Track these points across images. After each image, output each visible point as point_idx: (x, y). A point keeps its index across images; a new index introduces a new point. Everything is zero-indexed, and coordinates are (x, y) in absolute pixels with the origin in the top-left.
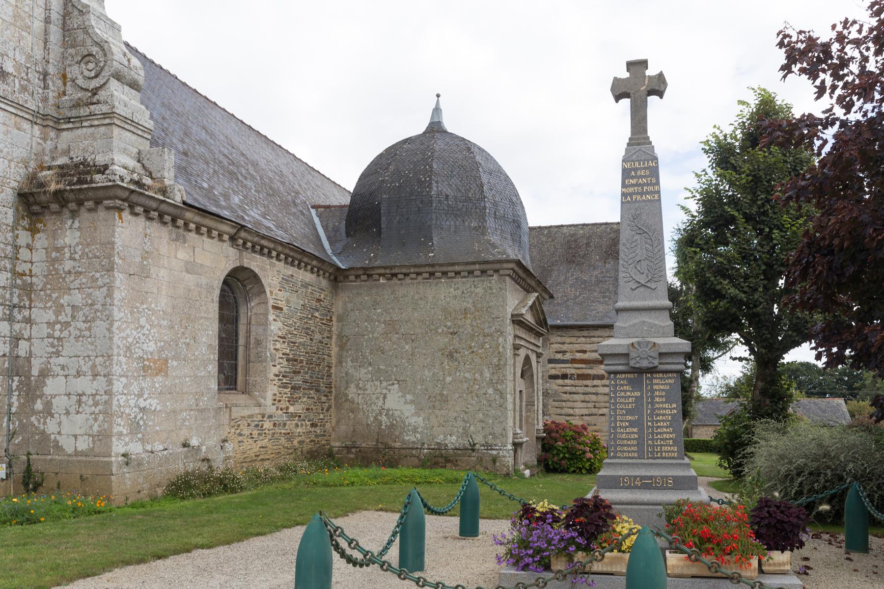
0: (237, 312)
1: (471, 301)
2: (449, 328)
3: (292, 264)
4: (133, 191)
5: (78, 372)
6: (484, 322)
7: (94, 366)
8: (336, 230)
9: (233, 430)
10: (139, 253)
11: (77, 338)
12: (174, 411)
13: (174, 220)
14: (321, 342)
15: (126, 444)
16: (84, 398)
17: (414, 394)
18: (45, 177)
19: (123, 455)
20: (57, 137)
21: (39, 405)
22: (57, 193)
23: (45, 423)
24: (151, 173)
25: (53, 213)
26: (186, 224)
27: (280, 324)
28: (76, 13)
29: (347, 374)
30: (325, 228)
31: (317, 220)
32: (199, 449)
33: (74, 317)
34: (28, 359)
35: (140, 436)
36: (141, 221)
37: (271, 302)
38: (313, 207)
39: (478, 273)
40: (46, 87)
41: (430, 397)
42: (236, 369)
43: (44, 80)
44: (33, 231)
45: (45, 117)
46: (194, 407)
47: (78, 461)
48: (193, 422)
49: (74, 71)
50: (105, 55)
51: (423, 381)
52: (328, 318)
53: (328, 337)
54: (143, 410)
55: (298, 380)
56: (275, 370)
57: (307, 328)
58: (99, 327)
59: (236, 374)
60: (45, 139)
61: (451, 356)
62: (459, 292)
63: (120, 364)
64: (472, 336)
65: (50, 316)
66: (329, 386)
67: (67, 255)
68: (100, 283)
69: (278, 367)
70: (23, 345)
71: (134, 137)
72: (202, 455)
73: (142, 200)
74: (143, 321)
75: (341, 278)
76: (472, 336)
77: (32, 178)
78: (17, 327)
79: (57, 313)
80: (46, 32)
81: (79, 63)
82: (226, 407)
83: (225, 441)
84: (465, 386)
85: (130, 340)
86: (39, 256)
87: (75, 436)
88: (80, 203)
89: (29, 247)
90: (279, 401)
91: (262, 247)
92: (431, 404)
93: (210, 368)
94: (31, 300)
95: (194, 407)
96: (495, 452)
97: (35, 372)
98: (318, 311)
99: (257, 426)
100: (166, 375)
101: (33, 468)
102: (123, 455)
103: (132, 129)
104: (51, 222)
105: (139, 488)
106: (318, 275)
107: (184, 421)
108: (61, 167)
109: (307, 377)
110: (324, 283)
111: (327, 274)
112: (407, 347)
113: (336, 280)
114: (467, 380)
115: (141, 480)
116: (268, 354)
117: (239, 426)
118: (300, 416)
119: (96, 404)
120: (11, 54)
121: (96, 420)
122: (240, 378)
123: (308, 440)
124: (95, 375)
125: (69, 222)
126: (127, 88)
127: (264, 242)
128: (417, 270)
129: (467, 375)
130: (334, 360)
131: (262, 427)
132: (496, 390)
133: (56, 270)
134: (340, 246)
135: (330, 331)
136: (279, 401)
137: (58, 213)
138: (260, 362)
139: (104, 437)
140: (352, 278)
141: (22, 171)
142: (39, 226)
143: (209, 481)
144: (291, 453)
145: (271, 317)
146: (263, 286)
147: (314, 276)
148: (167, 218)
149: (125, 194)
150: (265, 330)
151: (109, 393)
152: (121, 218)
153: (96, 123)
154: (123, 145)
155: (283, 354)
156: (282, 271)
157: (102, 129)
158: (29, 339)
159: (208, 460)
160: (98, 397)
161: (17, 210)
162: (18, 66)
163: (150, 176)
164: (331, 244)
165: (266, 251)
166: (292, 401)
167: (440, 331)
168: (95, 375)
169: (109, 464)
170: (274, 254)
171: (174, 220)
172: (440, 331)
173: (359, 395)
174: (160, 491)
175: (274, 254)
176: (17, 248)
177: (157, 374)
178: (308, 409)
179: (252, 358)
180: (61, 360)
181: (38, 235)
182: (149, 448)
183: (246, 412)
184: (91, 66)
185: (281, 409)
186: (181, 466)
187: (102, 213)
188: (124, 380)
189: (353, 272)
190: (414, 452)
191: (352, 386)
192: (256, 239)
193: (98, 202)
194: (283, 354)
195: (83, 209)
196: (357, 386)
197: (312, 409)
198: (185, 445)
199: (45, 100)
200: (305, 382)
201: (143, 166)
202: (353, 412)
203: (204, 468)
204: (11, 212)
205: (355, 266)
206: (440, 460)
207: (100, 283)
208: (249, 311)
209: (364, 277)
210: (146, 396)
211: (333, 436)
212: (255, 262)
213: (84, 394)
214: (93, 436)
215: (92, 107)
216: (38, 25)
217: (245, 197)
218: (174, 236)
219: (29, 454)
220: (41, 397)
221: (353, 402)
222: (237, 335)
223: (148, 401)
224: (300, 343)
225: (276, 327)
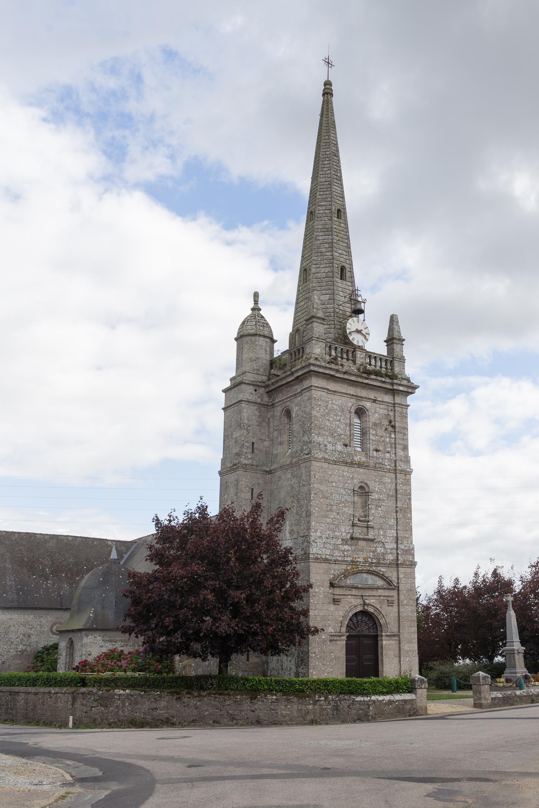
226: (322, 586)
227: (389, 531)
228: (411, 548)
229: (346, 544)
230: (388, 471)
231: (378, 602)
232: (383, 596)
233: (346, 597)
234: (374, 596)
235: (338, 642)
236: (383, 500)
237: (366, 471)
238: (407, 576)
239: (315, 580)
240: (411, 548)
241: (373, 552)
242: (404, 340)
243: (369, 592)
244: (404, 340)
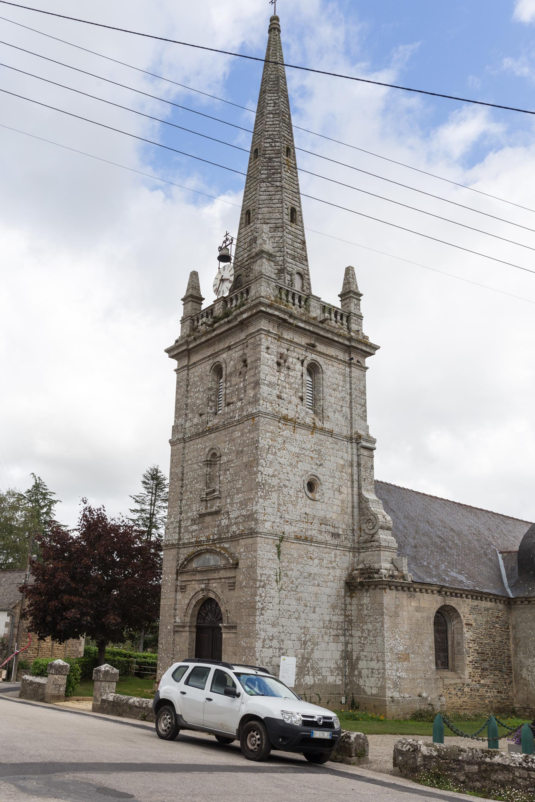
0: (446, 627)
3: (477, 599)
4: (389, 581)
5: (371, 659)
7: (377, 657)
8: (513, 569)
9: (445, 691)
10: (394, 606)
11: (370, 644)
12: (413, 679)
13: (409, 589)
14: (501, 642)
15: (392, 693)
16: (374, 671)
18: (355, 574)
19: (391, 697)
20: (359, 555)
21: (356, 673)
22: (360, 582)
23: (359, 681)
24: (397, 569)
25: (359, 590)
26: (415, 590)
27: (471, 633)
28: (364, 501)
29: (520, 661)
30: (506, 568)
31: (501, 562)
32: (426, 698)
33: (369, 635)
34: (351, 652)
35: (398, 689)
36: (394, 592)
37: (464, 622)
38: (500, 553)
40: (354, 535)
42: (448, 658)
43: (353, 532)
44: (351, 597)
45: (354, 548)
46: (423, 677)
47: (373, 699)
48: (423, 685)
49: (364, 526)
50: (376, 519)
52: (506, 627)
53: (506, 639)
54: (399, 677)
55: (486, 665)
56: (470, 659)
57: (490, 634)
58: (379, 639)
59: (448, 661)
60: (354, 557)
63: (388, 656)
65: (359, 634)
66: (510, 669)
67: (365, 608)
68: (378, 620)
69: (472, 657)
70: (349, 645)
71: (390, 553)
72: (429, 702)
73: (394, 584)
74: (397, 636)
75: (512, 603)
77: (350, 575)
78: (347, 638)
79: (362, 633)
80: (353, 512)
81: (366, 523)
82: (441, 678)
83: (441, 696)
85: (392, 645)
86: (354, 607)
87: (371, 687)
88: (369, 586)
89: (350, 604)
90: (474, 676)
91: (456, 594)
93: (431, 658)
94: (351, 626)
95: (423, 677)
97: (354, 658)
98: (497, 623)
99: (460, 689)
100: (409, 661)
101: (355, 700)
102: (391, 697)
103: (389, 550)
104: (358, 594)
105: (398, 713)
106: (496, 603)
107: (419, 684)
108: (361, 569)
109: (492, 663)
110: (501, 606)
111: (502, 601)
113: (509, 603)
115: (399, 710)
116: (464, 650)
117: (449, 688)
118: (489, 686)
119: (379, 674)
120: (341, 527)
121: (379, 680)
122: (450, 663)
123: (496, 701)
124: (378, 661)
125: (365, 594)
126: (385, 531)
127: (456, 591)
130: (512, 653)
131: (463, 690)
133: (361, 614)
134: (513, 581)
135: (508, 635)
136: (474, 676)
137: (361, 590)
138: (460, 654)
139: (382, 688)
140: (519, 603)
141: (346, 573)
142: (354, 595)
143: (432, 715)
144: (484, 708)
145: (465, 630)
146: (458, 613)
147: (493, 604)
148: (406, 589)
149: (387, 583)
150: (462, 637)
151: (384, 669)
152: (385, 592)
153: (374, 549)
154: (385, 558)
155: (474, 650)
156: (471, 604)
157: (376, 552)
158: (351, 644)
159: (432, 705)
160: (380, 671)
161: (345, 589)
162: (343, 531)
163: (397, 570)
164: (508, 580)
165: (459, 595)
166: (482, 677)
168: (378, 661)
169: (385, 701)
170: (464, 596)
171: (409, 589)
173: (529, 675)
174: (408, 717)
175: (464, 596)
176: (346, 605)
177: (404, 661)
178: (494, 682)
179: (456, 652)
180: (364, 653)
181: (353, 599)
182: (402, 695)
183: (453, 682)
184: (371, 524)
185: (475, 681)
186: (418, 706)
187: (378, 591)
188: (390, 663)
189: (519, 599)
191: (524, 669)
192: (452, 591)
193: (376, 586)
194: (474, 650)
195: (370, 588)
196: (527, 669)
197: (497, 682)
198: (420, 696)
199: (354, 540)
200: (491, 666)
201: (394, 565)
202: (526, 686)
203: (430, 708)
204: (343, 590)
205: (519, 596)
207: (378, 620)
208: (453, 626)
209: (526, 602)
210: (400, 671)
211: (515, 700)
212: (453, 602)
213: (374, 669)
214: (378, 688)
215: (372, 543)
216: (350, 510)
217: (449, 563)
218: (409, 596)
219: (353, 694)
220: (357, 669)
221: (525, 680)
222: (447, 639)
223: (401, 673)
224: (486, 643)
225: (468, 634)
226: (171, 574)
227: (236, 496)
228: (254, 511)
229: (195, 524)
230: (238, 423)
231: (220, 585)
232: (224, 578)
233: (191, 583)
234: (215, 579)
235: (183, 634)
236: (231, 461)
237: (217, 433)
238: (247, 549)
239: (166, 568)
240: (254, 511)
241: (218, 527)
242: (204, 299)
243: (211, 575)
244: (204, 299)
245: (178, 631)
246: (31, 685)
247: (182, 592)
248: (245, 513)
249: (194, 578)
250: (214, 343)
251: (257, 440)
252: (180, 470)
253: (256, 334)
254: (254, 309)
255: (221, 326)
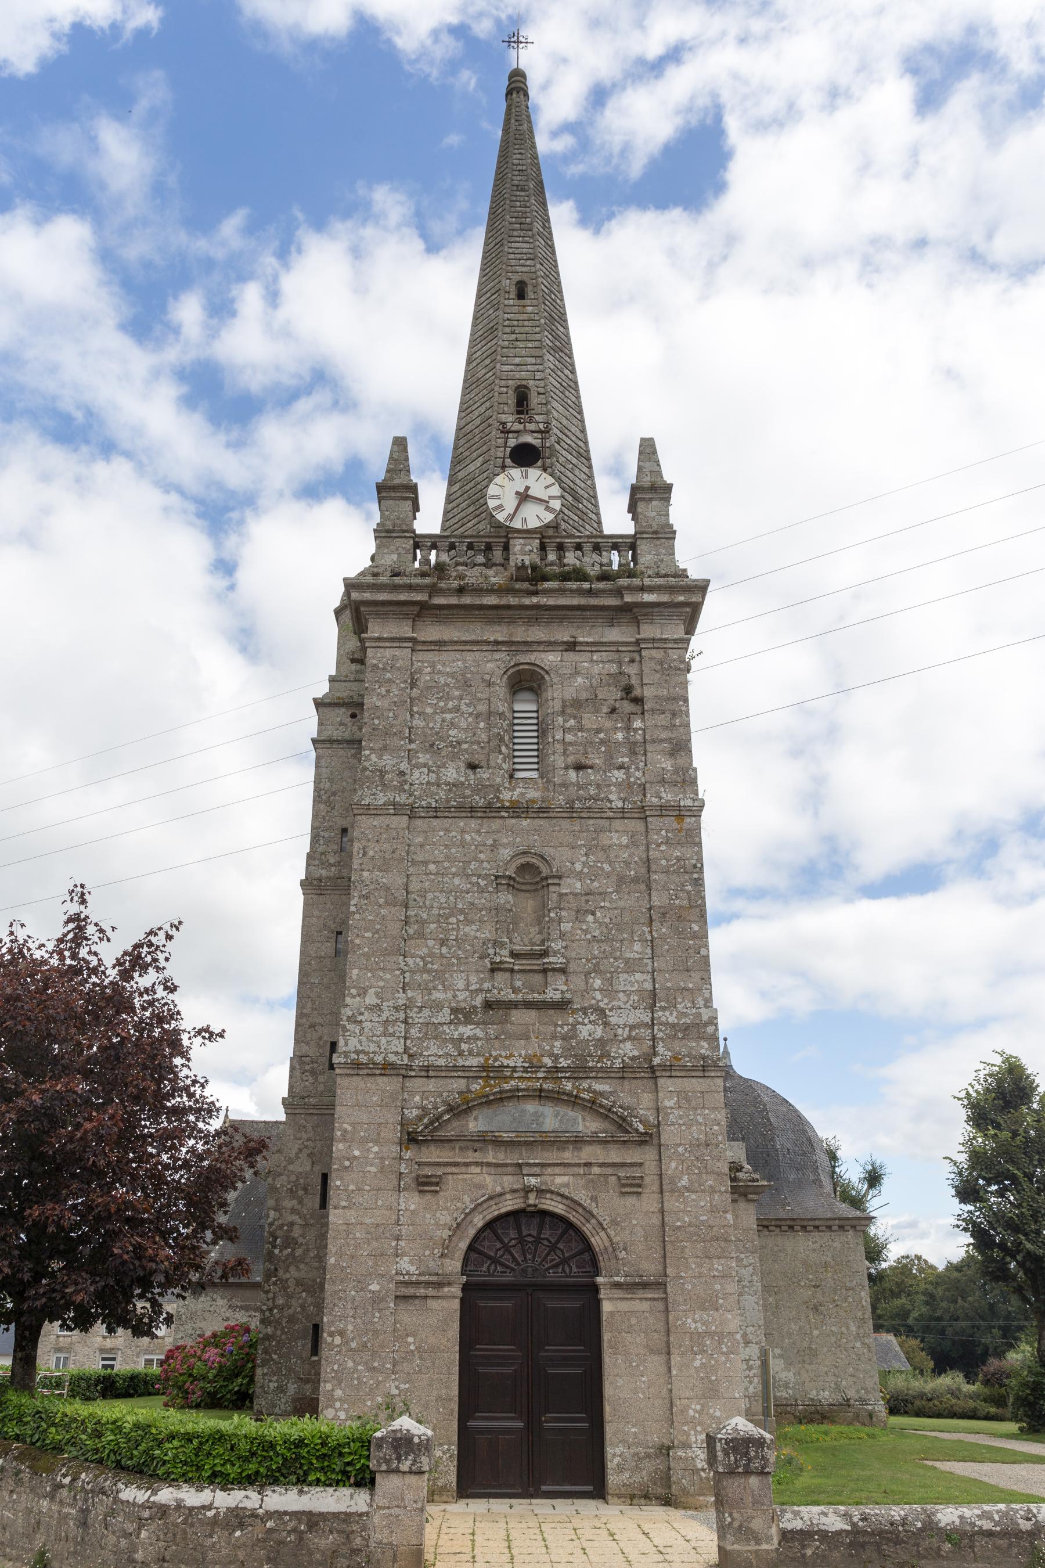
1: (830, 1255)
2: (811, 1281)
6: (845, 1276)
17: (782, 1348)
39: (835, 1228)
41: (798, 1352)
51: (790, 1335)
61: (815, 1309)
62: (818, 1246)
64: (835, 1290)
68: (745, 1262)
76: (835, 1290)
84: (833, 1339)
92: (800, 1358)
96: (870, 1407)
112: (771, 1299)
114: (834, 1334)
121: (751, 1382)
128: (778, 1223)
129: (833, 1328)
132: (863, 1344)
160: (751, 1362)
167: (802, 1284)
172: (802, 1284)
190: (789, 1409)
206: (817, 1416)
207: (745, 1262)
214: (749, 1397)
237: (542, 822)
239: (352, 1124)
241: (564, 1038)
245: (406, 1298)
246: (241, 1526)
247: (420, 1192)
248: (672, 1019)
249: (477, 1157)
250: (512, 621)
251: (695, 866)
252: (401, 880)
253: (670, 646)
254: (681, 595)
255: (562, 591)
